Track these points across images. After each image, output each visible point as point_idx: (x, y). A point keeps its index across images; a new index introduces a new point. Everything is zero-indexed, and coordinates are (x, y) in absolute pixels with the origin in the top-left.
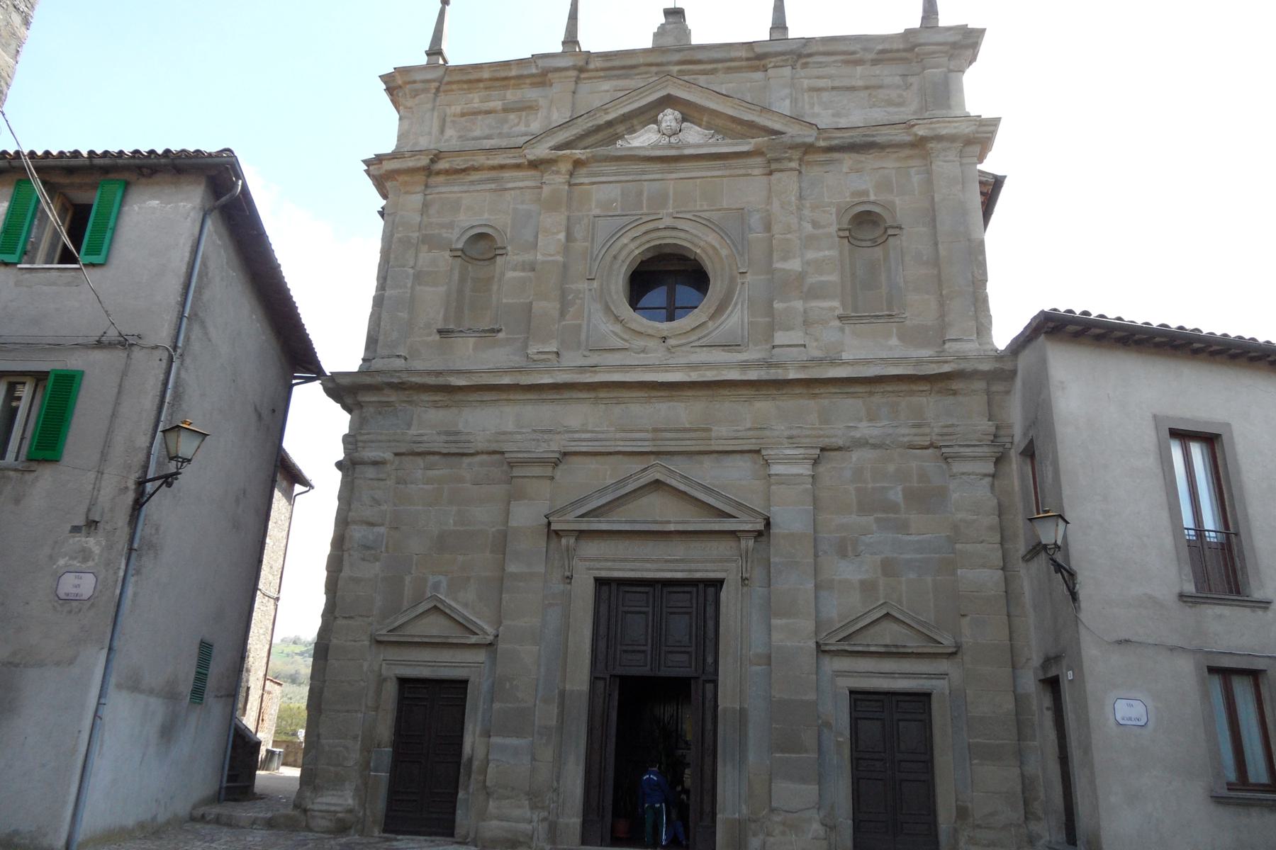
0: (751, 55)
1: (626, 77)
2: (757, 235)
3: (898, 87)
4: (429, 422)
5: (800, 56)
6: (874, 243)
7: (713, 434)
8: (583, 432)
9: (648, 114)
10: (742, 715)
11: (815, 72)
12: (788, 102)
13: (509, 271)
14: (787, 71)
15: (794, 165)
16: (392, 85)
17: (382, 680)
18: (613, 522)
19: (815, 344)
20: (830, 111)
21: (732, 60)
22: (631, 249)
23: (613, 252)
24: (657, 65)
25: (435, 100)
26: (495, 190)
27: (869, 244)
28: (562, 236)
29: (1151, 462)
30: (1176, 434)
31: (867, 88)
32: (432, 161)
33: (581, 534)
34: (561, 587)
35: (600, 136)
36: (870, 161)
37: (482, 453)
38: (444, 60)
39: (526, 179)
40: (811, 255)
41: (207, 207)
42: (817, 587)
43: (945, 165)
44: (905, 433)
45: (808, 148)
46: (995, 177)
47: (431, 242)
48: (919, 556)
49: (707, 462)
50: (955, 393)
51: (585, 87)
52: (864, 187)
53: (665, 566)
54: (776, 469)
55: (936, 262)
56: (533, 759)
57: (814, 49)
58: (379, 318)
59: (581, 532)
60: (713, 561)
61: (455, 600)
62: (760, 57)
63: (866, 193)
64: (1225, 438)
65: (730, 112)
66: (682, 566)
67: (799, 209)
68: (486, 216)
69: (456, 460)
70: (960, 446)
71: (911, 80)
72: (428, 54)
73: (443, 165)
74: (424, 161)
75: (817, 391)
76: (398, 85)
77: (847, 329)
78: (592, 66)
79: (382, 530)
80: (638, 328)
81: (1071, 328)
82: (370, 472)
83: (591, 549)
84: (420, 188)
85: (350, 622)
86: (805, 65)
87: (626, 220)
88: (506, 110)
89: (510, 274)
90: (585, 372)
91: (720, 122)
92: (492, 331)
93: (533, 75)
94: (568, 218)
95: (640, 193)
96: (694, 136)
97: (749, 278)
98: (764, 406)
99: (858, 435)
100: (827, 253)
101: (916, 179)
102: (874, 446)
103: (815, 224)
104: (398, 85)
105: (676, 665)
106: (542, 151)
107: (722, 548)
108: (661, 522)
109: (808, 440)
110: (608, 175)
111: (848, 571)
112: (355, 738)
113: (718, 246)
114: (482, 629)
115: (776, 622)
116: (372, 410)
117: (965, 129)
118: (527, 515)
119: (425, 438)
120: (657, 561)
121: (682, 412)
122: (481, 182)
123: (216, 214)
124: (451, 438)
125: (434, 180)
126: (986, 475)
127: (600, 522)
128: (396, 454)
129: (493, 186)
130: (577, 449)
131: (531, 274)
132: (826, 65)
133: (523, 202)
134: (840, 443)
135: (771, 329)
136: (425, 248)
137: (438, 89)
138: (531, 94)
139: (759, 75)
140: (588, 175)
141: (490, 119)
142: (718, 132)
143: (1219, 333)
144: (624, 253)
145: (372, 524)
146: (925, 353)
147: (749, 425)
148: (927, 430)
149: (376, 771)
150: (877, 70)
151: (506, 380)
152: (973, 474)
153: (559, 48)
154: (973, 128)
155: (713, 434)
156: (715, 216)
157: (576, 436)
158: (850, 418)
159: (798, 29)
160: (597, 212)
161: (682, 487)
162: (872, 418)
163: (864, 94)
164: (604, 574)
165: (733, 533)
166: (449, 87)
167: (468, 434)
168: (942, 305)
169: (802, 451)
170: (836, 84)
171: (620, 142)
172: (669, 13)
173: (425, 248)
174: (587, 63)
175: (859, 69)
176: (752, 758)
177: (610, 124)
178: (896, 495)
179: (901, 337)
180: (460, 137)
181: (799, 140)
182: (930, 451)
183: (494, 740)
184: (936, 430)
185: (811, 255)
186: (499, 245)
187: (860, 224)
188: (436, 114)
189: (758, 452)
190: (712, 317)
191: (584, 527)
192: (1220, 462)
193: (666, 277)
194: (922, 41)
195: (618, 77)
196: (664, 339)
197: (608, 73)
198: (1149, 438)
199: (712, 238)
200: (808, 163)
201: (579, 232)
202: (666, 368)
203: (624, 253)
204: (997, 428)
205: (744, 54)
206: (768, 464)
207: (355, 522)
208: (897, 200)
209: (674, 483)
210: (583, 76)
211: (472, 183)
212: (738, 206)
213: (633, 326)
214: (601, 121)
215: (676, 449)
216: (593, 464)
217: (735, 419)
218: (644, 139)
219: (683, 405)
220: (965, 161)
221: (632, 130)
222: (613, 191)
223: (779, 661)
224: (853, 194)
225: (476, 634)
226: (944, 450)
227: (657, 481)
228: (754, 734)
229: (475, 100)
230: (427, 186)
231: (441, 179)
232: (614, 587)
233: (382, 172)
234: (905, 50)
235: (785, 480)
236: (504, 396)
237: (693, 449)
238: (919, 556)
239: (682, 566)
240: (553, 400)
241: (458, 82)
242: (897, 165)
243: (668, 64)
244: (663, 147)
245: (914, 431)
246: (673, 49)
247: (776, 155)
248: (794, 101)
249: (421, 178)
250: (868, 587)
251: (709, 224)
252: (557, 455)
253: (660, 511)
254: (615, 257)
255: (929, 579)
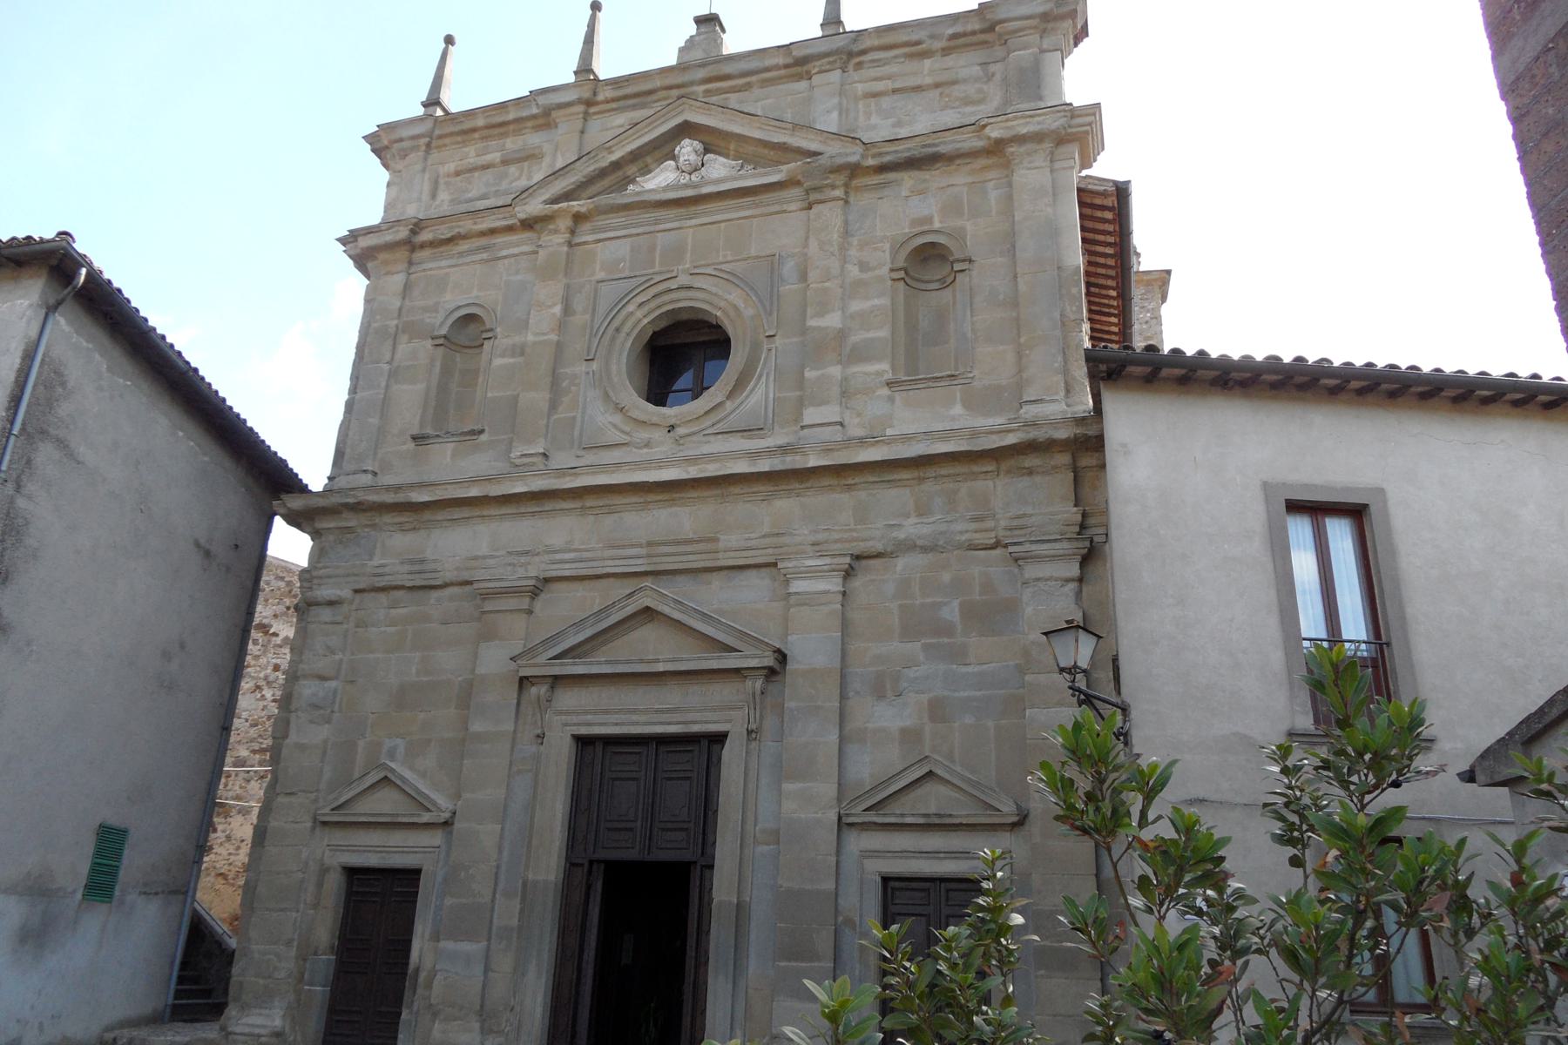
0: (789, 60)
1: (643, 106)
2: (790, 288)
3: (977, 80)
4: (393, 548)
5: (851, 55)
6: (945, 284)
7: (721, 545)
8: (570, 551)
9: (662, 148)
10: (741, 911)
11: (873, 72)
12: (835, 115)
13: (497, 360)
14: (836, 76)
15: (839, 193)
16: (377, 146)
17: (324, 870)
18: (591, 663)
19: (857, 420)
20: (890, 121)
21: (767, 70)
22: (641, 318)
23: (616, 323)
24: (678, 87)
25: (425, 159)
26: (487, 261)
27: (936, 286)
28: (557, 310)
29: (1257, 547)
30: (1294, 507)
31: (937, 86)
32: (414, 232)
33: (556, 681)
34: (534, 748)
35: (606, 182)
36: (935, 178)
37: (451, 584)
38: (444, 109)
39: (518, 244)
40: (856, 306)
41: (52, 301)
42: (842, 740)
43: (1031, 173)
44: (963, 529)
45: (854, 170)
46: (1115, 183)
47: (410, 329)
48: (978, 693)
49: (716, 581)
50: (1030, 472)
51: (595, 125)
52: (926, 212)
53: (656, 717)
54: (798, 586)
55: (1014, 303)
56: (487, 969)
57: (868, 43)
58: (348, 428)
59: (556, 678)
60: (714, 709)
61: (411, 768)
62: (803, 61)
63: (929, 220)
64: (1373, 509)
65: (757, 134)
66: (677, 717)
67: (843, 248)
68: (475, 293)
69: (421, 593)
70: (1032, 542)
71: (992, 68)
72: (425, 105)
73: (425, 236)
74: (403, 233)
75: (850, 481)
76: (385, 143)
77: (898, 396)
78: (600, 97)
79: (333, 684)
80: (642, 417)
81: (1355, 384)
82: (326, 614)
83: (569, 698)
84: (403, 266)
85: (293, 799)
86: (859, 65)
87: (635, 282)
88: (505, 162)
89: (498, 362)
90: (564, 475)
91: (750, 149)
92: (472, 432)
93: (534, 117)
94: (568, 287)
95: (652, 249)
96: (719, 170)
97: (778, 341)
98: (786, 506)
99: (902, 536)
100: (876, 302)
101: (994, 195)
102: (925, 549)
103: (863, 266)
104: (385, 143)
105: (668, 849)
106: (534, 207)
107: (724, 692)
108: (649, 662)
109: (838, 546)
110: (615, 229)
111: (887, 717)
112: (289, 943)
113: (742, 305)
114: (434, 804)
115: (788, 787)
116: (331, 538)
117: (1052, 123)
118: (495, 660)
119: (387, 570)
120: (646, 711)
121: (683, 518)
122: (471, 252)
123: (69, 306)
124: (417, 568)
125: (419, 255)
126: (1068, 580)
127: (575, 664)
128: (356, 591)
129: (485, 256)
130: (560, 573)
131: (520, 359)
132: (886, 62)
133: (517, 272)
134: (879, 547)
135: (801, 404)
136: (405, 338)
137: (428, 145)
138: (534, 139)
139: (803, 84)
140: (594, 231)
141: (488, 175)
142: (747, 161)
143: (1359, 362)
144: (629, 324)
145: (323, 678)
146: (998, 421)
147: (766, 530)
148: (990, 524)
149: (311, 984)
150: (950, 61)
151: (474, 492)
152: (1050, 579)
153: (571, 79)
154: (1062, 121)
155: (721, 545)
156: (738, 268)
157: (558, 556)
158: (892, 512)
159: (855, 18)
160: (601, 275)
161: (676, 615)
162: (922, 511)
163: (935, 93)
164: (583, 731)
165: (737, 671)
166: (440, 142)
167: (435, 561)
168: (1020, 355)
169: (828, 560)
170: (898, 85)
171: (631, 187)
172: (701, 21)
173: (404, 338)
174: (595, 94)
175: (927, 63)
176: (753, 966)
177: (616, 165)
178: (951, 612)
179: (967, 405)
180: (452, 201)
181: (840, 161)
182: (998, 552)
183: (442, 944)
184: (1003, 523)
185: (856, 306)
186: (488, 326)
187: (925, 260)
188: (427, 176)
189: (775, 565)
190: (730, 396)
191: (557, 671)
192: (1369, 544)
193: (680, 353)
194: (1002, 16)
195: (634, 107)
196: (672, 428)
197: (622, 103)
198: (1255, 514)
199: (735, 296)
200: (857, 189)
201: (579, 303)
202: (660, 464)
203: (629, 324)
204: (1084, 515)
205: (781, 61)
206: (787, 582)
207: (305, 677)
208: (969, 226)
209: (666, 610)
210: (592, 110)
211: (461, 254)
212: (769, 252)
213: (635, 414)
214: (604, 164)
215: (681, 566)
216: (579, 591)
217: (746, 524)
218: (661, 179)
219: (687, 509)
220: (1057, 165)
221: (646, 171)
222: (622, 249)
223: (780, 835)
224: (914, 223)
225: (429, 810)
226: (1011, 549)
227: (647, 609)
228: (757, 934)
229: (471, 154)
230: (410, 263)
231: (426, 253)
232: (599, 747)
233: (364, 249)
234: (983, 31)
235: (808, 600)
236: (477, 512)
237: (695, 565)
238: (978, 693)
239: (677, 717)
240: (533, 514)
241: (451, 134)
242: (970, 179)
243: (692, 83)
244: (686, 186)
245: (974, 526)
246: (706, 66)
247: (817, 183)
248: (843, 111)
249: (402, 254)
250: (910, 736)
251: (732, 279)
252: (532, 582)
253: (652, 648)
254: (617, 330)
255: (990, 724)
